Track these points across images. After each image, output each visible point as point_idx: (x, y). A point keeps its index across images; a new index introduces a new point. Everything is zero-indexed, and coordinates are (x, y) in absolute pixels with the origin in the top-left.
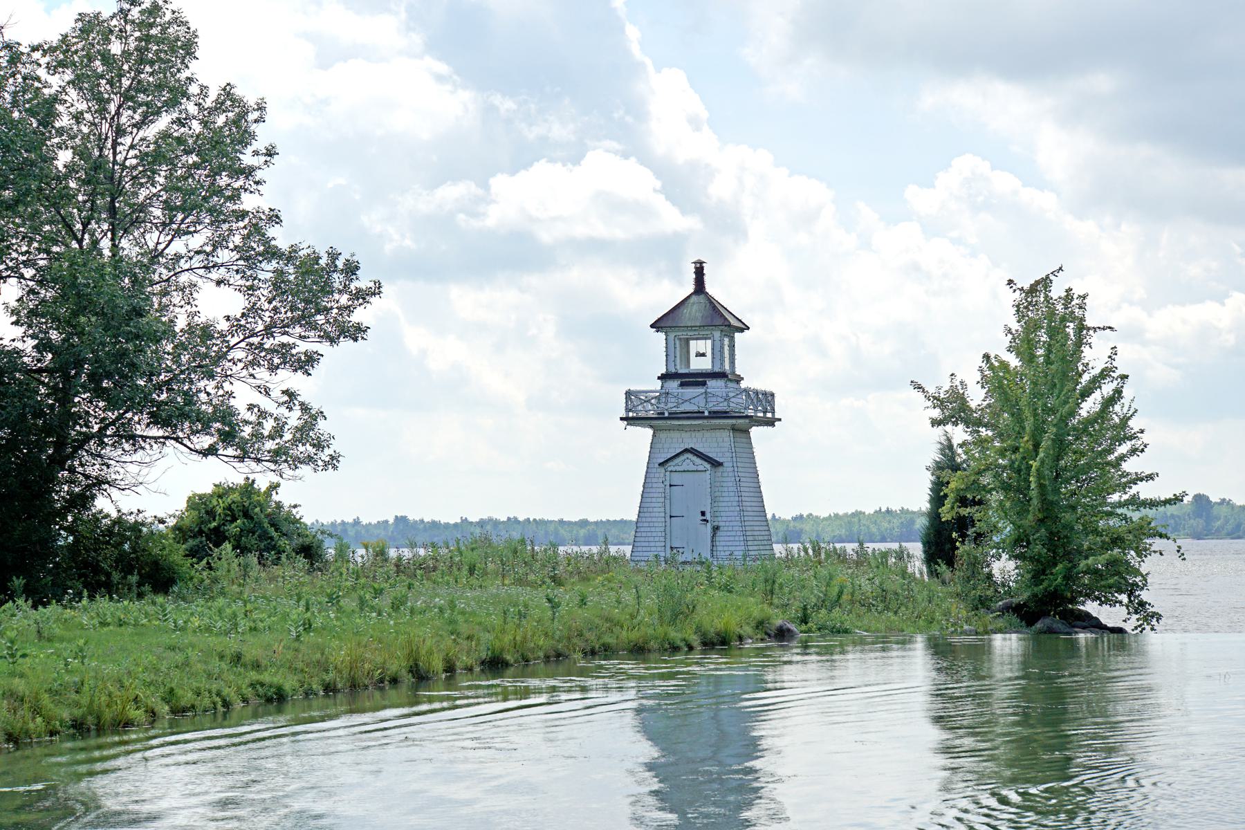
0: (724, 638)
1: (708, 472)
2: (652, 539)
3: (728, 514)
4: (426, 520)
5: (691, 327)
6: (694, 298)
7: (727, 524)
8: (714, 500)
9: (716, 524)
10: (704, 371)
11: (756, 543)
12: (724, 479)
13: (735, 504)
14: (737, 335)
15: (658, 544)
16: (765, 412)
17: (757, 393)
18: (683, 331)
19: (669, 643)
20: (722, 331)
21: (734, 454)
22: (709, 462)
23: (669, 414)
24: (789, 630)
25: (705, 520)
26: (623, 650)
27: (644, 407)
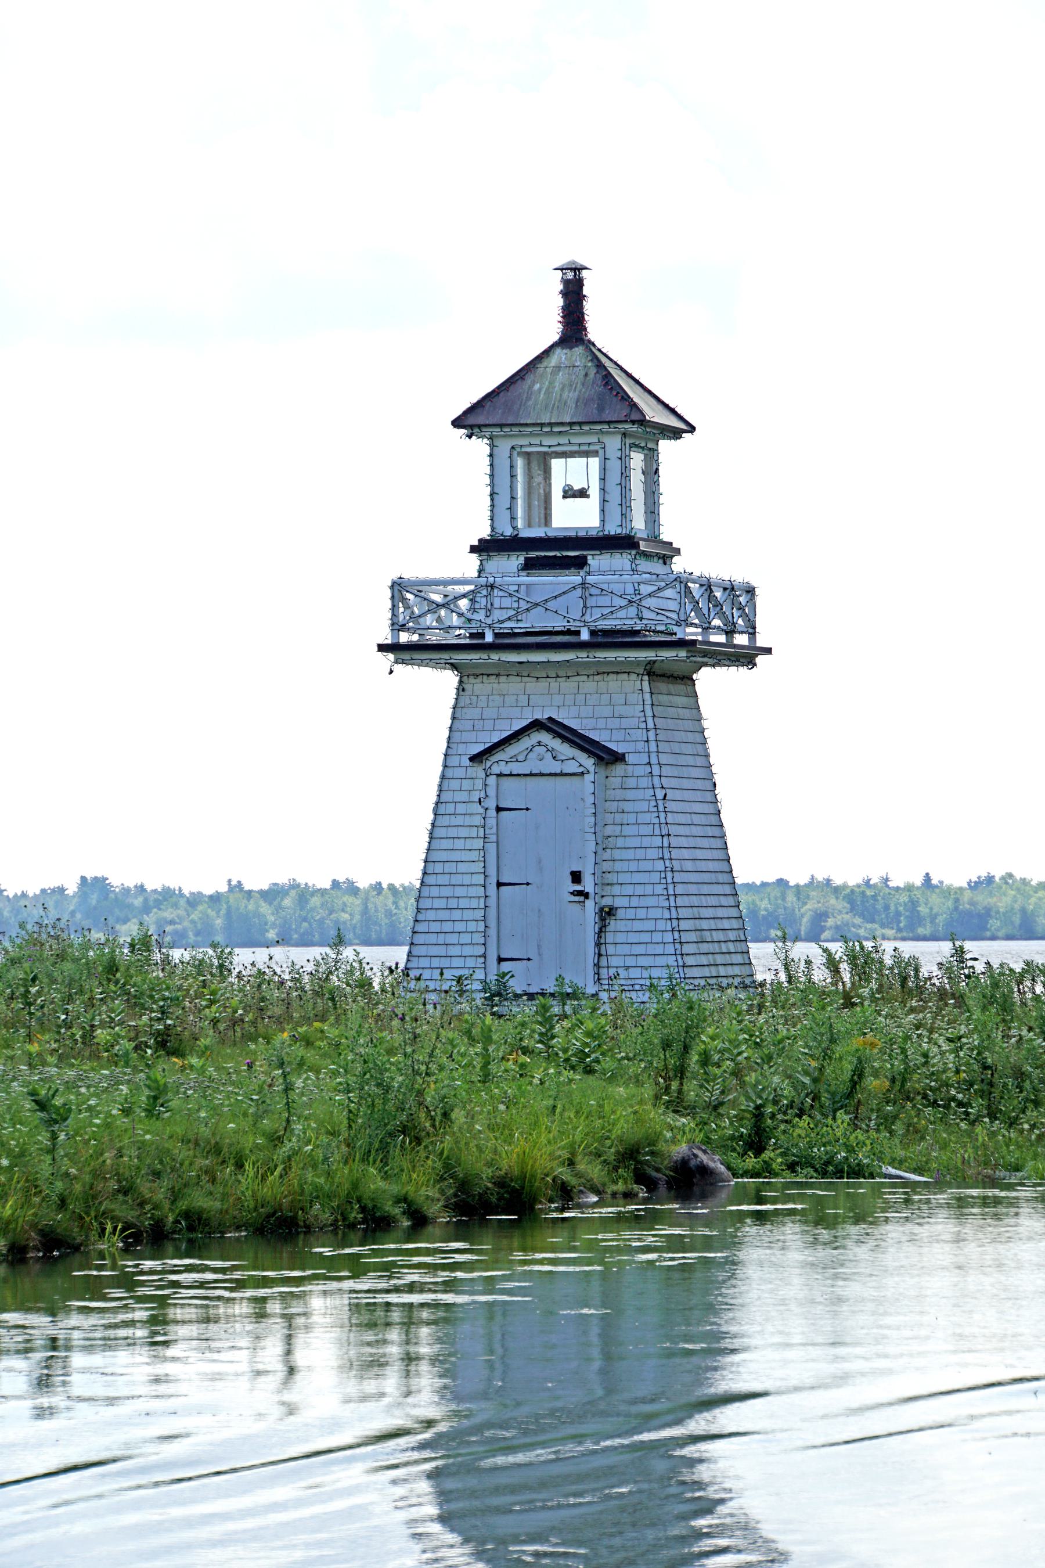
0: (516, 1194)
1: (589, 778)
2: (453, 939)
3: (637, 878)
4: (149, 887)
5: (551, 424)
6: (560, 356)
7: (635, 902)
8: (603, 845)
9: (607, 901)
10: (581, 534)
11: (705, 948)
12: (630, 795)
13: (653, 853)
14: (665, 446)
15: (468, 950)
16: (730, 633)
17: (708, 586)
18: (531, 434)
19: (363, 1209)
20: (624, 435)
21: (652, 735)
22: (590, 753)
23: (497, 635)
24: (704, 1171)
25: (580, 893)
26: (238, 1228)
27: (439, 619)
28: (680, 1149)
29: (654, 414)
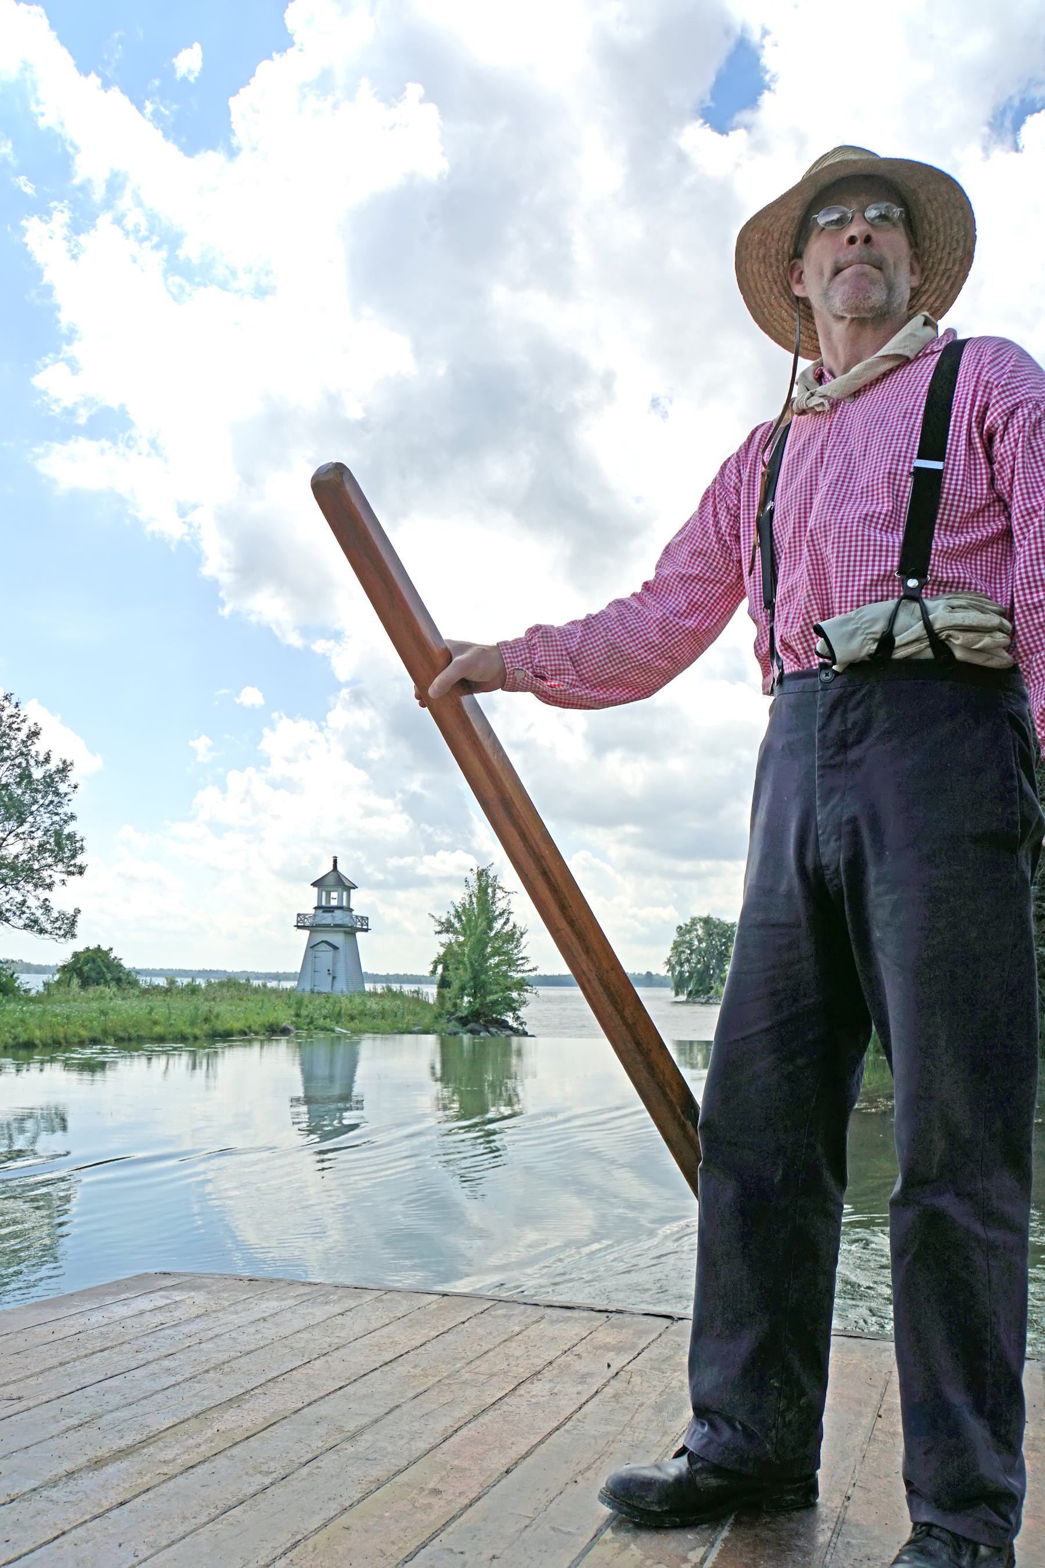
14: (352, 891)
24: (288, 1029)
28: (284, 1024)
29: (347, 884)
